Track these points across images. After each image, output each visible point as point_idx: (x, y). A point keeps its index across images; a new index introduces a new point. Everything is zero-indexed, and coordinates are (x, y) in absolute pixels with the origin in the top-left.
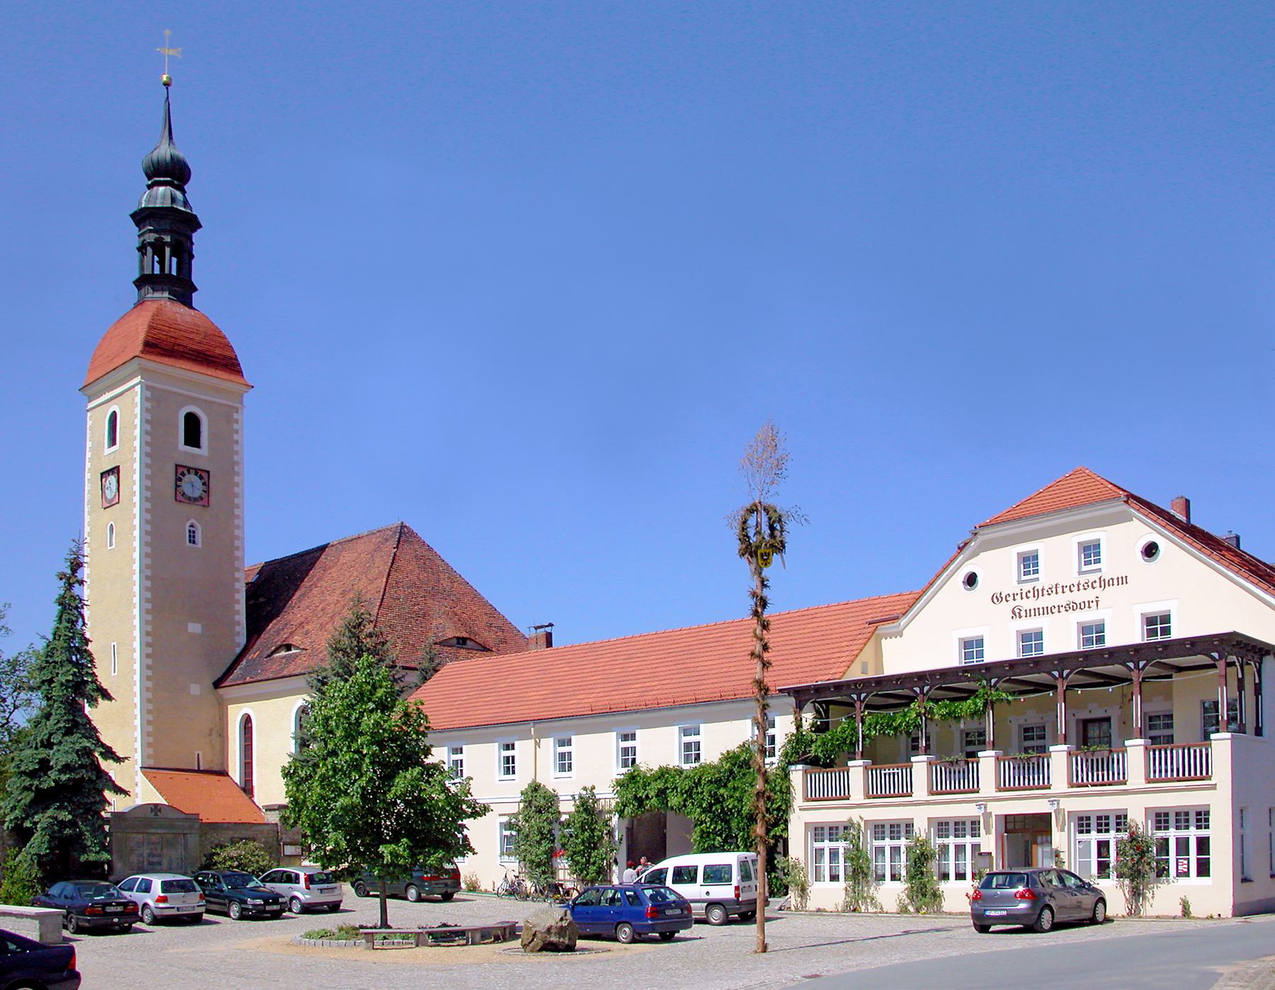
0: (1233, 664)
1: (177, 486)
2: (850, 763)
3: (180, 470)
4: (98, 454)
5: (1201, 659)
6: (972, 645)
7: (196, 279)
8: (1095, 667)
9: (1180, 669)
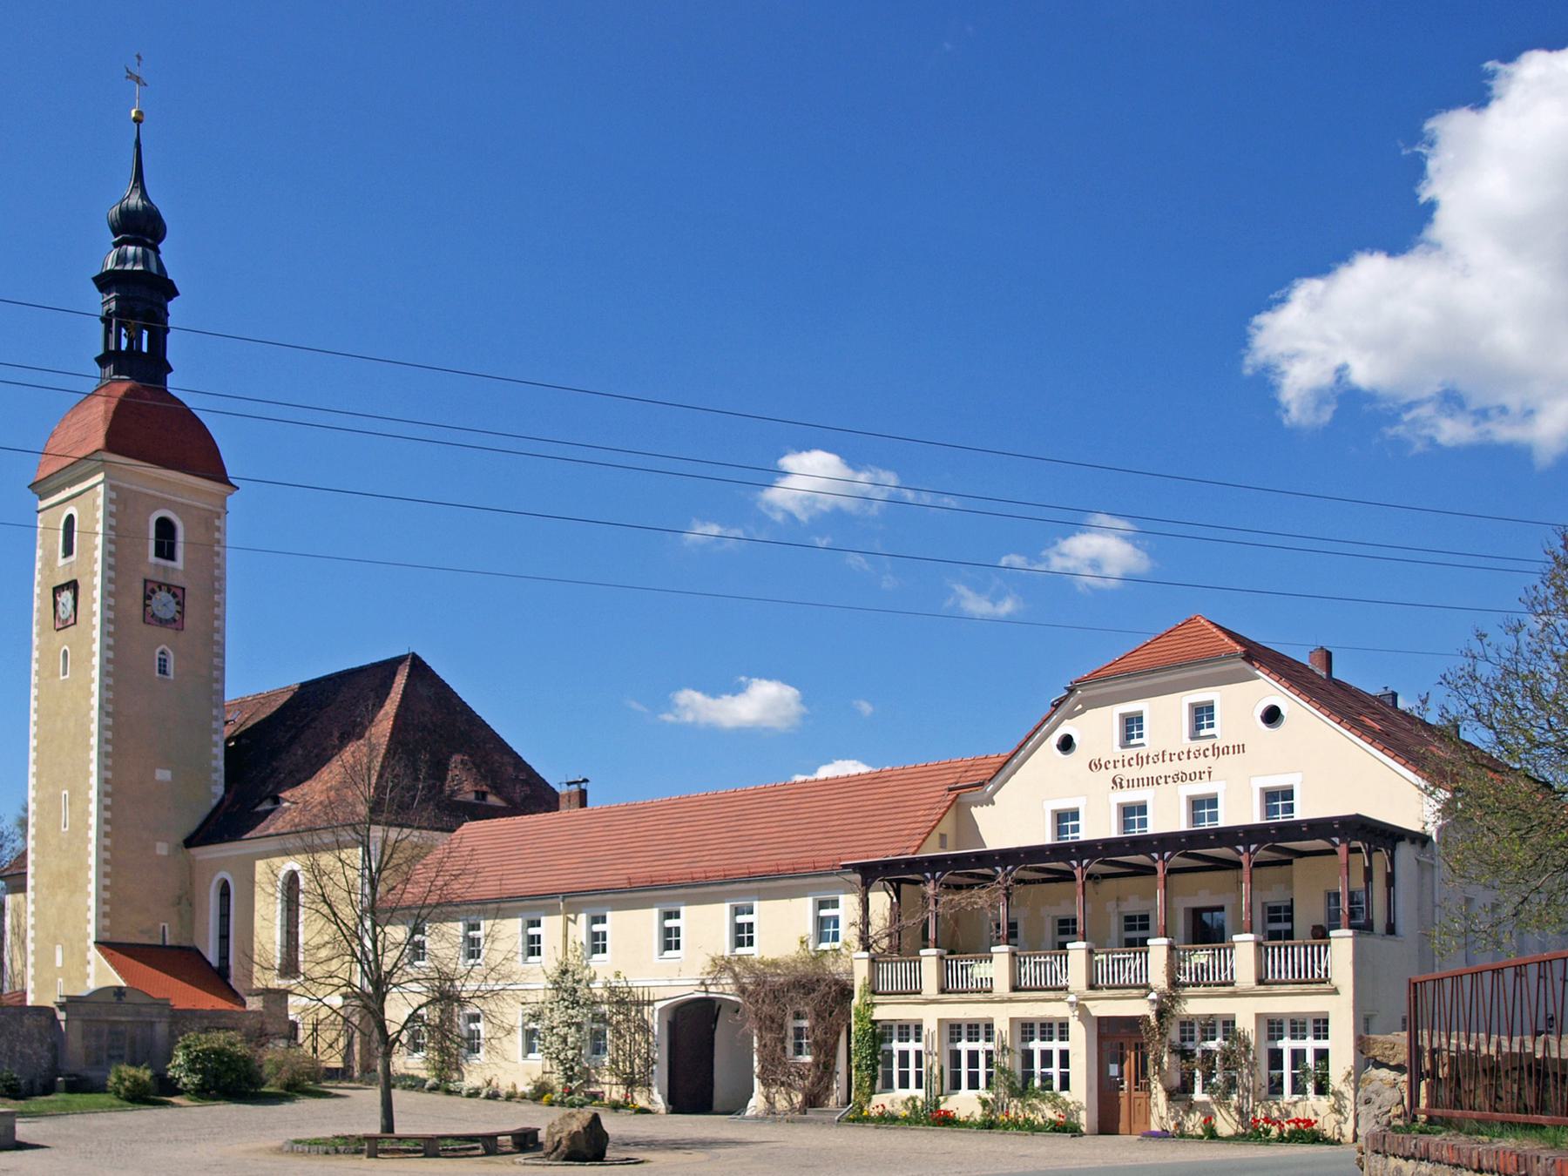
0: (1358, 850)
1: (145, 606)
2: (922, 952)
3: (150, 586)
4: (47, 564)
5: (1320, 844)
6: (1065, 818)
7: (170, 357)
8: (1204, 848)
9: (1302, 854)
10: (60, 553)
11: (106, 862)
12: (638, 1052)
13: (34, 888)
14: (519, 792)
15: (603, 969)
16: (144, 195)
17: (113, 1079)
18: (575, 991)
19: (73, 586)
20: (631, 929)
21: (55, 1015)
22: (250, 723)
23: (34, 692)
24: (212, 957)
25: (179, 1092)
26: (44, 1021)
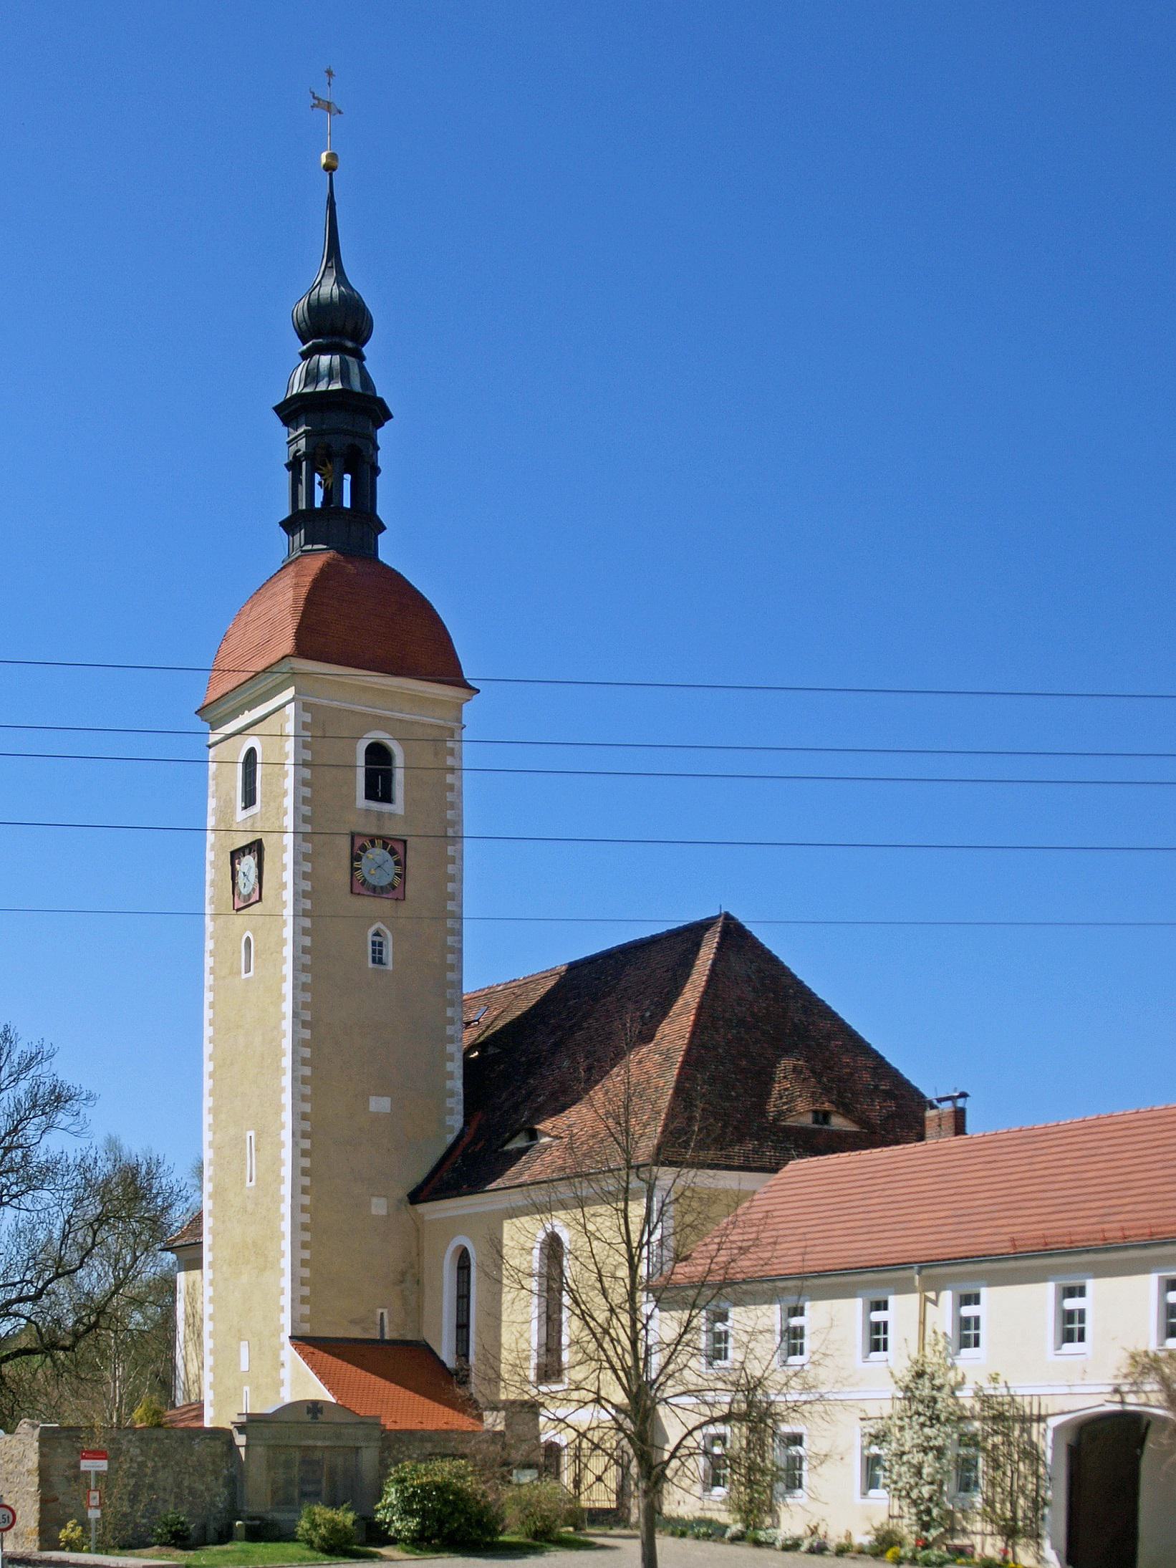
1: (353, 869)
3: (358, 842)
7: (382, 512)
10: (239, 803)
11: (305, 1228)
12: (1022, 1489)
13: (211, 1265)
14: (877, 1110)
15: (974, 1372)
16: (341, 279)
17: (304, 1524)
18: (934, 1400)
19: (256, 848)
20: (1017, 1312)
21: (232, 1440)
22: (500, 1024)
23: (208, 997)
24: (447, 1354)
25: (391, 1542)
26: (219, 1447)
